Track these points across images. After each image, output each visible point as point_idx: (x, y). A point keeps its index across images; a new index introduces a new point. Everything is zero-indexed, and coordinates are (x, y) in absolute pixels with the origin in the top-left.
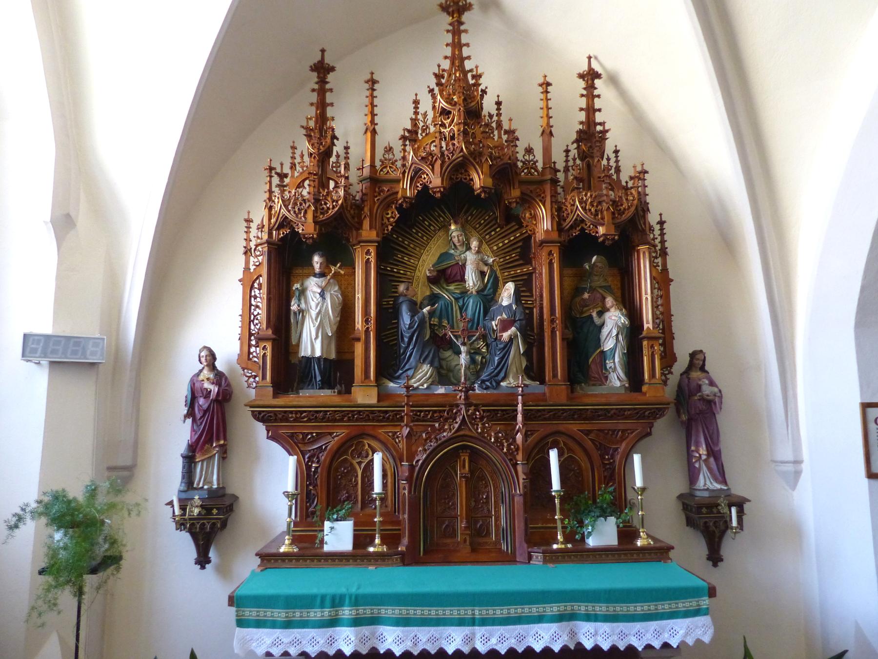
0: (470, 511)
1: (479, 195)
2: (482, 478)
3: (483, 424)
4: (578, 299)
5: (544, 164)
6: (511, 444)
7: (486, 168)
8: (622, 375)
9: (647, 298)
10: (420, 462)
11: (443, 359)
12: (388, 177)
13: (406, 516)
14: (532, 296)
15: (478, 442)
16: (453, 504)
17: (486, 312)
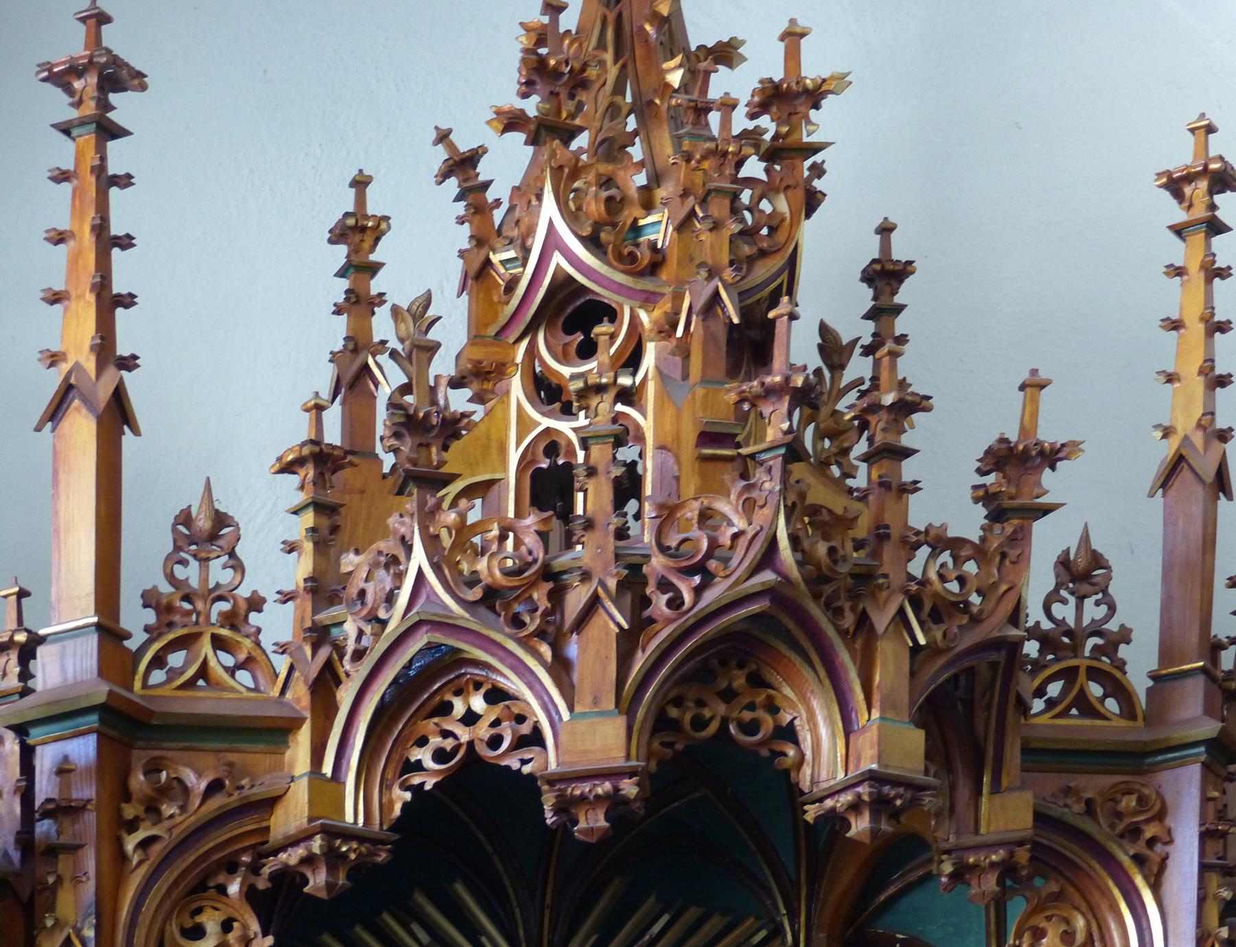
1: (836, 822)
5: (1167, 653)
7: (890, 666)
12: (204, 703)
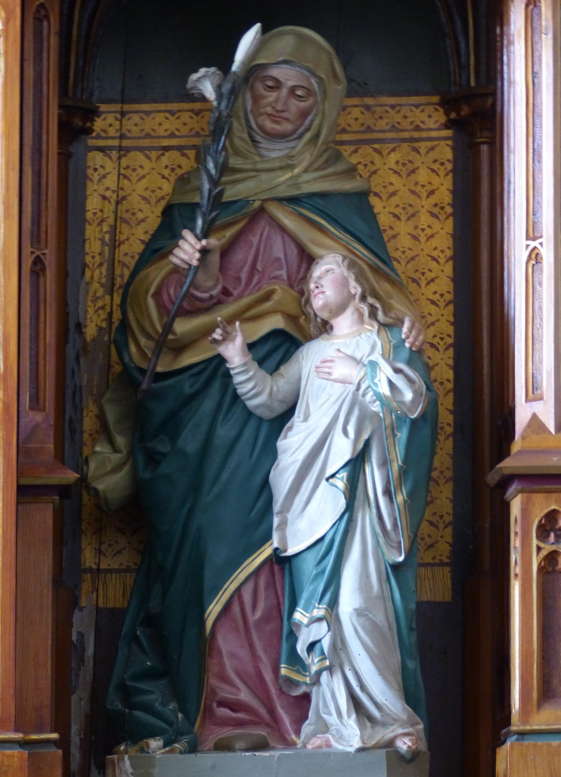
4: (156, 274)
8: (382, 692)
9: (535, 257)
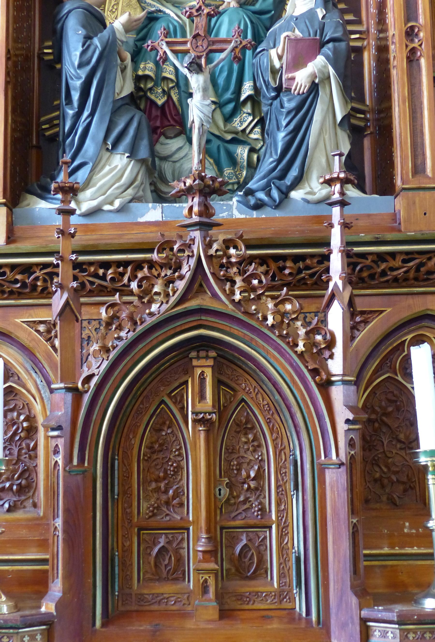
0: (218, 509)
2: (246, 426)
3: (247, 281)
6: (316, 330)
10: (95, 380)
11: (165, 159)
13: (59, 522)
14: (359, 22)
15: (236, 329)
16: (177, 494)
17: (258, 39)
